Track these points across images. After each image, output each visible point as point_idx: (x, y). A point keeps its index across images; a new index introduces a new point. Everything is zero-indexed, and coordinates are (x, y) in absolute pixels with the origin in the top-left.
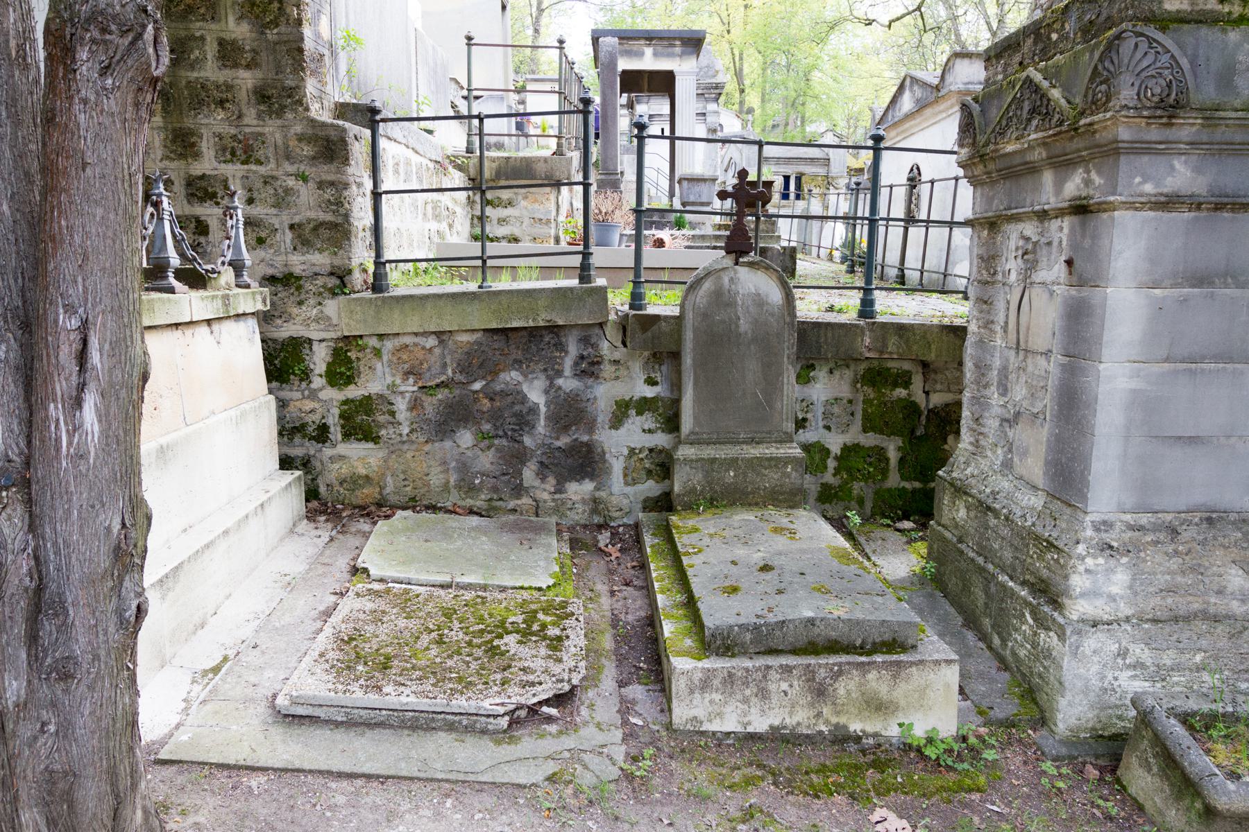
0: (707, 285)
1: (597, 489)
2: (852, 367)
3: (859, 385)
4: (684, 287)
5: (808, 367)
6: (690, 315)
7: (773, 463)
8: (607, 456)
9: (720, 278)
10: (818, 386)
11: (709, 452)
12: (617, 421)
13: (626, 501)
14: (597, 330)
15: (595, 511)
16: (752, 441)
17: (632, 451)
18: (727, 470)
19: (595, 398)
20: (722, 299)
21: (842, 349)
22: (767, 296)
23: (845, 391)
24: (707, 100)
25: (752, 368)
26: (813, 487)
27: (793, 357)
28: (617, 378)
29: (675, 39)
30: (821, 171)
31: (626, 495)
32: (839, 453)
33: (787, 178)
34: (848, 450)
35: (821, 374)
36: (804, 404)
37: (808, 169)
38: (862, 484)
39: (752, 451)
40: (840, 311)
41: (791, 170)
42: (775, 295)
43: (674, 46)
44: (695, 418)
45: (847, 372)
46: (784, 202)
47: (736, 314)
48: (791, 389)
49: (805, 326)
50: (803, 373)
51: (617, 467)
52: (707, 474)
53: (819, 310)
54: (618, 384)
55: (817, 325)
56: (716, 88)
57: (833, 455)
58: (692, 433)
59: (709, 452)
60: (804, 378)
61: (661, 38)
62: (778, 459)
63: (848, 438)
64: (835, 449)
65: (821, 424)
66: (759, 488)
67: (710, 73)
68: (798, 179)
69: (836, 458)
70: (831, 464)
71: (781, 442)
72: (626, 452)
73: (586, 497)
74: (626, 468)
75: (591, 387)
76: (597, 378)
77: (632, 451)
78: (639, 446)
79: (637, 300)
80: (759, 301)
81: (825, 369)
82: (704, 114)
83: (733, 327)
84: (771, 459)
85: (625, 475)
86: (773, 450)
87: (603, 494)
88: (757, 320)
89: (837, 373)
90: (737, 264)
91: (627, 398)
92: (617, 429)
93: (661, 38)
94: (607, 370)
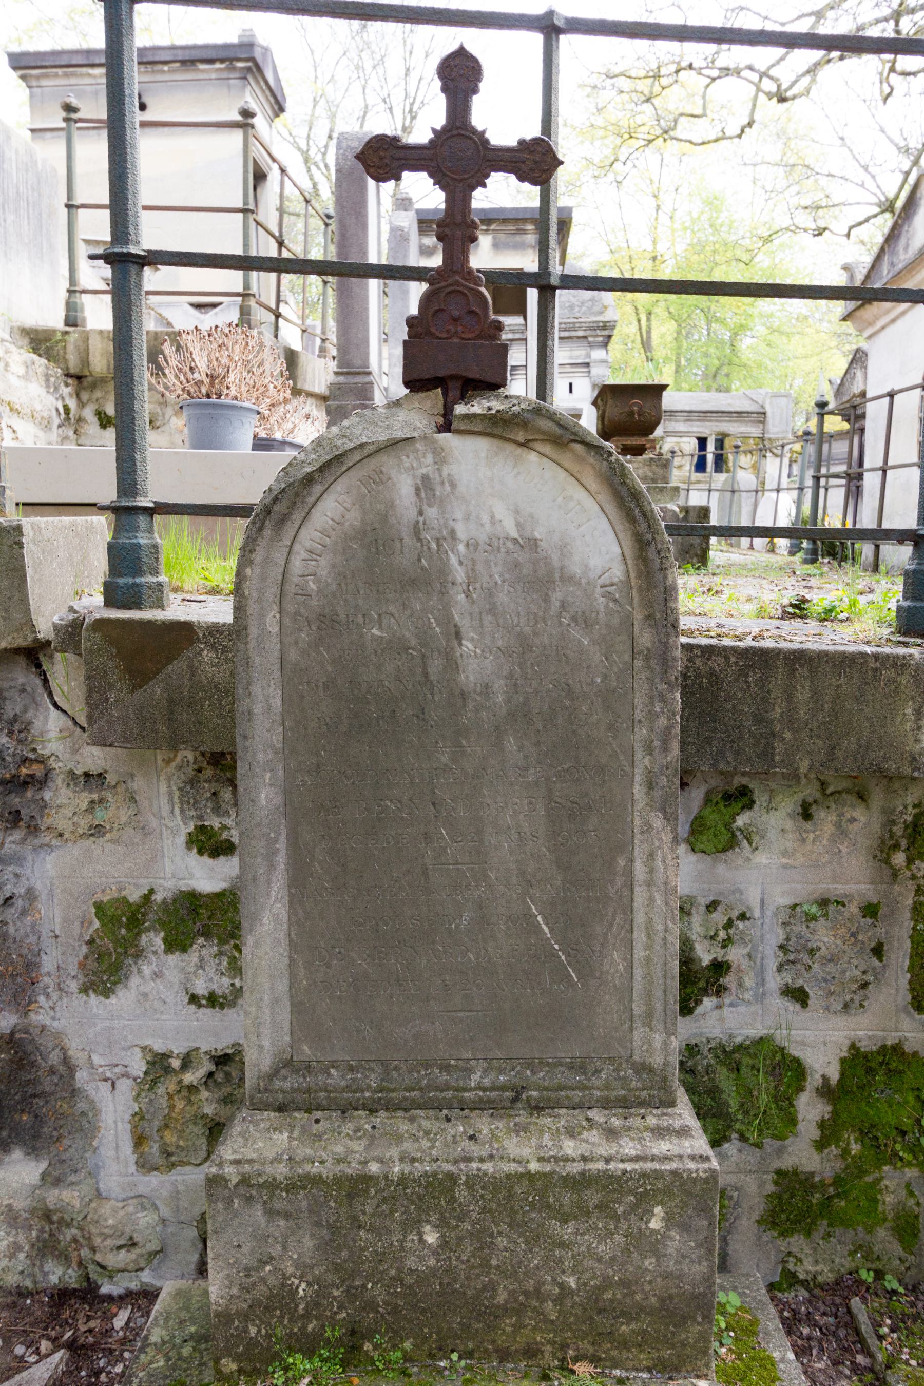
0: (332, 508)
1: (51, 1179)
2: (877, 798)
3: (899, 859)
4: (242, 523)
5: (728, 797)
6: (268, 622)
7: (593, 1198)
8: (81, 1076)
9: (379, 479)
10: (761, 858)
11: (342, 1148)
12: (106, 968)
13: (146, 1219)
14: (22, 676)
15: (47, 1247)
16: (516, 1101)
17: (159, 1064)
18: (414, 1224)
19: (31, 895)
20: (391, 562)
21: (849, 744)
22: (563, 549)
23: (854, 878)
24: (591, 345)
25: (510, 825)
26: (750, 1184)
27: (668, 782)
28: (97, 831)
29: (525, 220)
30: (754, 430)
31: (145, 1202)
32: (834, 1075)
33: (702, 442)
34: (866, 1068)
35: (772, 819)
36: (719, 917)
37: (733, 428)
38: (911, 1173)
39: (514, 1146)
40: (828, 616)
41: (709, 430)
42: (596, 547)
43: (524, 232)
44: (297, 1007)
45: (859, 813)
46: (700, 476)
47: (447, 621)
48: (668, 871)
49: (717, 663)
50: (712, 817)
51: (113, 1111)
52: (334, 1238)
53: (761, 614)
54: (99, 847)
55: (759, 660)
56: (604, 328)
57: (813, 1081)
58: (286, 1064)
59: (342, 1148)
60: (716, 830)
61: (505, 221)
62: (611, 1184)
63: (868, 1028)
64: (822, 1057)
65: (774, 982)
66: (538, 1293)
67: (596, 309)
68: (720, 444)
69: (826, 1091)
70: (810, 1109)
71: (625, 1104)
72: (138, 1067)
73: (21, 1204)
74: (139, 1116)
75: (18, 859)
76: (33, 829)
77: (159, 1064)
78: (178, 1048)
79: (128, 570)
80: (535, 568)
81: (788, 804)
82: (587, 365)
83: (435, 665)
84: (582, 1182)
85: (139, 1140)
86: (594, 1142)
87: (68, 1197)
88: (525, 644)
89: (826, 819)
90: (446, 427)
91: (134, 896)
92: (107, 993)
93: (505, 221)
94: (63, 803)
